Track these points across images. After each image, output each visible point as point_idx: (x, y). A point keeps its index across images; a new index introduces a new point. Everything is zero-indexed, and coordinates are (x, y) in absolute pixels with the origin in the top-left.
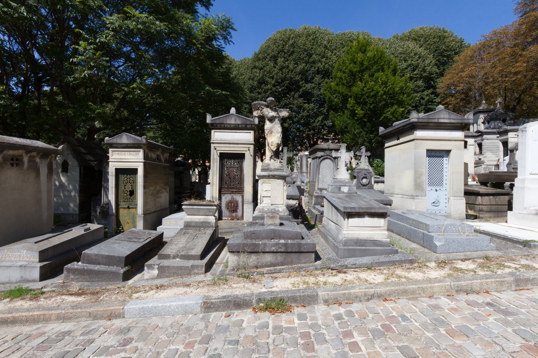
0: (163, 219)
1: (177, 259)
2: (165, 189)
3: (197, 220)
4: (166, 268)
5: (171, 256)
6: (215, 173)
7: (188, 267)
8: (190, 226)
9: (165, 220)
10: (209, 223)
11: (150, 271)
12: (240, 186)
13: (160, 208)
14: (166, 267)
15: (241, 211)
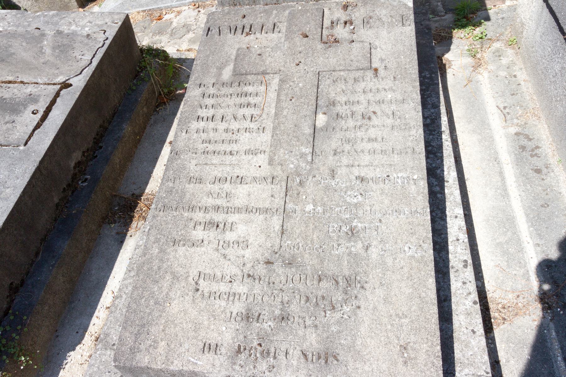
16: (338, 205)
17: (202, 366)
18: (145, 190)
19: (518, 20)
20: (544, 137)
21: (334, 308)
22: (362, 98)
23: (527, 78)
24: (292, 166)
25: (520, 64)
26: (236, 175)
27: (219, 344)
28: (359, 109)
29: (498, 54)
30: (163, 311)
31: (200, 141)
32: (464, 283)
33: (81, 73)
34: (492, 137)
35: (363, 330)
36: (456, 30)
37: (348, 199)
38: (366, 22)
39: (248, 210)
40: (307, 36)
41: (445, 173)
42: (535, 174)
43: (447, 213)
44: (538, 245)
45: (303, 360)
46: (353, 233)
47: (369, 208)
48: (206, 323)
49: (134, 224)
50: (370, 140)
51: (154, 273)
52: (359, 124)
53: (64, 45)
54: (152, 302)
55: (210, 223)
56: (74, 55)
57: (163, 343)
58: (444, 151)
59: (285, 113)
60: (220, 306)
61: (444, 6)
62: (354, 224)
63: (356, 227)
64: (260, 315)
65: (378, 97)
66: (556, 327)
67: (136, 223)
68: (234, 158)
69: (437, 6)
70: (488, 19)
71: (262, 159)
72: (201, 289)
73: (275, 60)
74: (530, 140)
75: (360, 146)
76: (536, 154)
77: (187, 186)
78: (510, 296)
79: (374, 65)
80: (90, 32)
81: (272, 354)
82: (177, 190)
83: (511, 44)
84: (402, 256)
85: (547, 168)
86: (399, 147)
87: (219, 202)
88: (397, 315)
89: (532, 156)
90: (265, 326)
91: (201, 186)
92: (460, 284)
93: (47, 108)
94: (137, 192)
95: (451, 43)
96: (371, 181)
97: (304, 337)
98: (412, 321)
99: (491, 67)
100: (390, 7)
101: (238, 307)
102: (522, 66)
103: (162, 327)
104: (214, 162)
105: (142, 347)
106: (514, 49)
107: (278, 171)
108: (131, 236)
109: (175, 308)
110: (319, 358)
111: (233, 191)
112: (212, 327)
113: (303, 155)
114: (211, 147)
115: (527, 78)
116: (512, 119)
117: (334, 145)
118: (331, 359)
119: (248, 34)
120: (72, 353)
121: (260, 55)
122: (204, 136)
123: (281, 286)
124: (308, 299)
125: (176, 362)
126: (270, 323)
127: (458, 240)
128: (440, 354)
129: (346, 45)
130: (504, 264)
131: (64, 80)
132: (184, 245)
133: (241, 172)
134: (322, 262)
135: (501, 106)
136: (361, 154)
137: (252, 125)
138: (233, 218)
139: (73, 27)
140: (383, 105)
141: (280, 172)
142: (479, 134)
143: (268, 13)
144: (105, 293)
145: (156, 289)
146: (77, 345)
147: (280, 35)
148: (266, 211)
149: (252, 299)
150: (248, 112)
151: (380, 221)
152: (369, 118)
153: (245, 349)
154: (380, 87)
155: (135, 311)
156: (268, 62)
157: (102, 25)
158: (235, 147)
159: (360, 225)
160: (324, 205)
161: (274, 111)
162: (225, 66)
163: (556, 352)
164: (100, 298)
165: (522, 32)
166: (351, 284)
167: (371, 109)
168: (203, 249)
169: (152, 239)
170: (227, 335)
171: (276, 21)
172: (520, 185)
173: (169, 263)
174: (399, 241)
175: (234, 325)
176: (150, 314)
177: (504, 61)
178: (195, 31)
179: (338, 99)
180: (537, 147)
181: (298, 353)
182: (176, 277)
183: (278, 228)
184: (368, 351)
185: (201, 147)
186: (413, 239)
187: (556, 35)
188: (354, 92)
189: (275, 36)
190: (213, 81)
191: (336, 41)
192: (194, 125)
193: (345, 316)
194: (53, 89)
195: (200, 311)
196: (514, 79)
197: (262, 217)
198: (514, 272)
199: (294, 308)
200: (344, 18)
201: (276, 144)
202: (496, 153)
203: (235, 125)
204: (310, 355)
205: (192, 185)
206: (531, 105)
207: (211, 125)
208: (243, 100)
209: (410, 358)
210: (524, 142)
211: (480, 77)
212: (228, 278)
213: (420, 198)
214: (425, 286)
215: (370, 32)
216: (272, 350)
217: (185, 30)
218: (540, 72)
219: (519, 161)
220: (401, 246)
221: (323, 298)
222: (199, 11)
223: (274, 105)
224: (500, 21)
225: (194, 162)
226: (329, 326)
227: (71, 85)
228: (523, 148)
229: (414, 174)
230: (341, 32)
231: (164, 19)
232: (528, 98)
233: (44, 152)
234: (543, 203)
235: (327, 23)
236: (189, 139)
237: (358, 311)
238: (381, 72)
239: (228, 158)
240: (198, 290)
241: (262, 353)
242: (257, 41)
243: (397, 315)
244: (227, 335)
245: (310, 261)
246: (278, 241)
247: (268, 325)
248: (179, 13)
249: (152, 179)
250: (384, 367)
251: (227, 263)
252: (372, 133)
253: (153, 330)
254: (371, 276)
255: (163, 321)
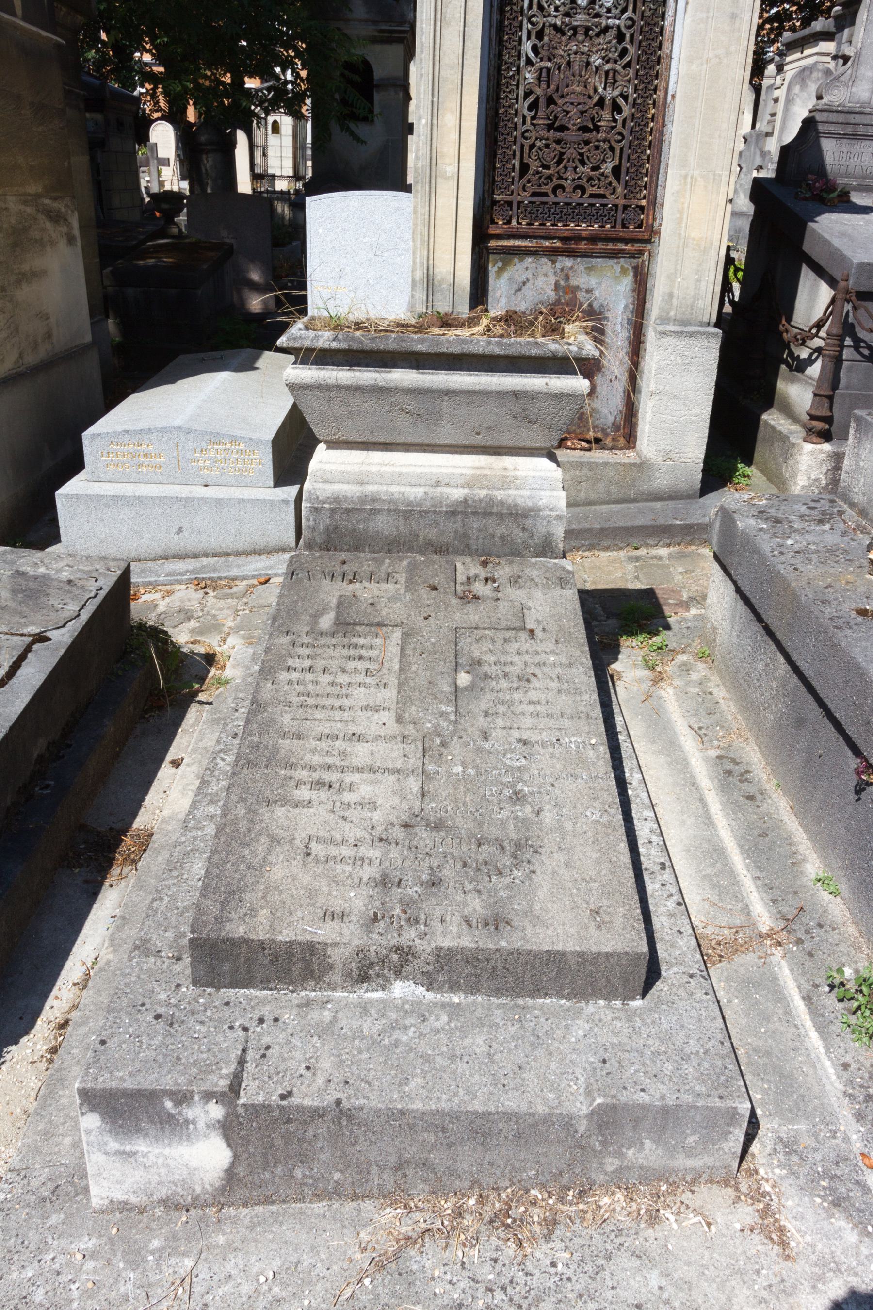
0: (86, 435)
1: (401, 989)
2: (56, 218)
3: (416, 493)
4: (321, 1128)
5: (336, 955)
6: (450, 75)
7: (568, 1123)
8: (358, 543)
9: (100, 437)
10: (519, 515)
11: (141, 1146)
12: (631, 189)
13: (43, 352)
14: (317, 1114)
15: (621, 386)
16: (495, 768)
17: (324, 935)
18: (132, 823)
19: (709, 626)
20: (756, 760)
21: (501, 873)
22: (516, 659)
23: (727, 696)
24: (429, 725)
25: (715, 679)
26: (351, 732)
27: (347, 911)
28: (515, 670)
29: (686, 669)
30: (261, 876)
31: (295, 693)
32: (663, 885)
33: (64, 626)
34: (685, 760)
35: (542, 894)
36: (624, 637)
37: (508, 762)
38: (515, 581)
39: (372, 770)
40: (436, 589)
41: (627, 775)
42: (747, 801)
43: (634, 815)
44: (759, 878)
45: (465, 926)
46: (518, 798)
47: (536, 772)
48: (325, 889)
49: (116, 870)
50: (531, 702)
51: (241, 836)
52: (515, 685)
53: (31, 590)
54: (242, 867)
55: (318, 783)
56: (50, 603)
57: (265, 911)
58: (623, 753)
59: (414, 668)
60: (344, 871)
61: (604, 608)
62: (519, 788)
63: (520, 791)
64: (400, 880)
65: (537, 659)
66: (789, 965)
67: (119, 869)
68: (346, 714)
69: (595, 608)
70: (668, 627)
71: (387, 717)
72: (314, 854)
73: (395, 611)
74: (738, 764)
75: (518, 709)
76: (746, 780)
77: (280, 741)
78: (726, 932)
79: (529, 626)
80: (72, 578)
81: (422, 921)
82: (266, 747)
83: (701, 657)
84: (584, 820)
85: (762, 794)
86: (569, 712)
87: (329, 760)
88: (584, 879)
89: (741, 781)
90: (410, 891)
91: (301, 742)
92: (658, 886)
93: (14, 663)
94: (118, 826)
95: (618, 652)
96: (536, 746)
97: (465, 904)
98: (603, 885)
99: (677, 682)
100: (544, 569)
101: (369, 872)
102: (719, 682)
103: (260, 894)
104: (318, 717)
105: (233, 915)
106: (706, 662)
107: (410, 730)
108: (111, 886)
109: (278, 872)
110: (487, 924)
111: (349, 749)
112: (335, 893)
113: (442, 714)
114: (311, 701)
115: (727, 696)
116: (711, 741)
117: (484, 706)
118: (502, 925)
119: (351, 582)
120: (13, 1048)
121: (372, 604)
122: (300, 688)
123: (428, 849)
124: (465, 865)
125: (285, 932)
126: (415, 889)
127: (650, 842)
128: (641, 917)
129: (490, 604)
130: (715, 898)
131: (38, 631)
132: (283, 806)
133: (360, 730)
134: (480, 825)
135: (696, 726)
136: (522, 717)
137: (368, 680)
138: (349, 778)
139: (42, 570)
140: (544, 668)
141: (413, 731)
142: (669, 756)
143: (379, 562)
144: (69, 964)
145: (247, 852)
146: (22, 1036)
147: (398, 586)
148: (398, 771)
149: (388, 864)
150: (361, 665)
151: (553, 785)
152: (528, 681)
153: (383, 917)
154: (539, 649)
155: (218, 877)
156: (384, 613)
157: (90, 572)
158: (346, 703)
159: (526, 789)
160: (477, 767)
161: (397, 667)
162: (322, 614)
163: (792, 992)
164: (61, 970)
165: (715, 640)
166: (522, 850)
167: (530, 670)
168: (311, 810)
169: (234, 798)
170: (357, 902)
171: (390, 570)
172: (728, 814)
173: (264, 825)
174: (579, 806)
175: (365, 891)
176: (239, 880)
177: (694, 676)
178: (201, 619)
179: (484, 658)
180: (747, 772)
181: (457, 919)
182: (274, 840)
183: (416, 789)
184: (549, 915)
185: (296, 700)
186: (597, 804)
187: (753, 628)
188: (505, 652)
189: (390, 586)
190: (306, 629)
191: (476, 597)
192: (283, 676)
193: (517, 881)
194: (20, 642)
195: (315, 877)
196: (709, 696)
197: (392, 778)
198: (730, 907)
199: (448, 872)
200: (483, 574)
201: (404, 700)
202: (693, 777)
203: (343, 679)
204: (475, 921)
205: (287, 741)
206: (735, 726)
207: (309, 677)
208: (352, 652)
209: (603, 923)
210: (731, 766)
211: (663, 693)
212: (352, 841)
213: (601, 763)
214: (615, 851)
215: (519, 592)
216: (423, 917)
217: (182, 616)
218: (742, 681)
219: (724, 788)
220: (581, 810)
221: (486, 863)
222: (206, 593)
223: (397, 660)
224: (685, 631)
225: (287, 717)
226: (496, 891)
227: (49, 639)
228: (729, 773)
229: (591, 739)
230: (479, 588)
231: (140, 601)
232: (730, 718)
233: (16, 716)
234: (760, 831)
235: (461, 578)
236: (277, 691)
237: (533, 876)
238: (539, 633)
239: (338, 715)
240: (309, 854)
241: (409, 920)
242: (366, 591)
243: (584, 879)
244: (357, 902)
245: (465, 825)
246: (418, 803)
247: (413, 891)
248: (169, 593)
249: (143, 809)
250: (572, 931)
251: (348, 825)
252: (533, 695)
253: (247, 896)
254: (546, 841)
255: (262, 887)
